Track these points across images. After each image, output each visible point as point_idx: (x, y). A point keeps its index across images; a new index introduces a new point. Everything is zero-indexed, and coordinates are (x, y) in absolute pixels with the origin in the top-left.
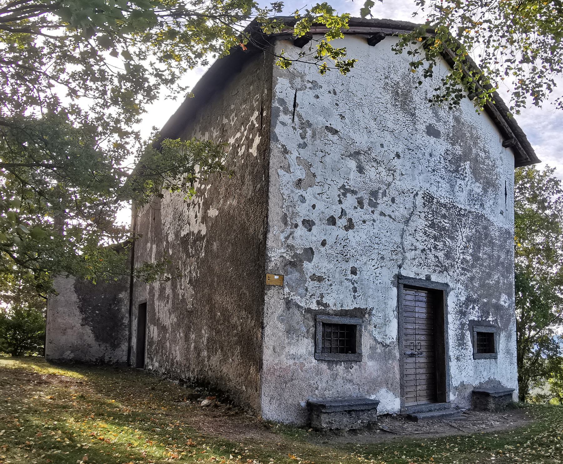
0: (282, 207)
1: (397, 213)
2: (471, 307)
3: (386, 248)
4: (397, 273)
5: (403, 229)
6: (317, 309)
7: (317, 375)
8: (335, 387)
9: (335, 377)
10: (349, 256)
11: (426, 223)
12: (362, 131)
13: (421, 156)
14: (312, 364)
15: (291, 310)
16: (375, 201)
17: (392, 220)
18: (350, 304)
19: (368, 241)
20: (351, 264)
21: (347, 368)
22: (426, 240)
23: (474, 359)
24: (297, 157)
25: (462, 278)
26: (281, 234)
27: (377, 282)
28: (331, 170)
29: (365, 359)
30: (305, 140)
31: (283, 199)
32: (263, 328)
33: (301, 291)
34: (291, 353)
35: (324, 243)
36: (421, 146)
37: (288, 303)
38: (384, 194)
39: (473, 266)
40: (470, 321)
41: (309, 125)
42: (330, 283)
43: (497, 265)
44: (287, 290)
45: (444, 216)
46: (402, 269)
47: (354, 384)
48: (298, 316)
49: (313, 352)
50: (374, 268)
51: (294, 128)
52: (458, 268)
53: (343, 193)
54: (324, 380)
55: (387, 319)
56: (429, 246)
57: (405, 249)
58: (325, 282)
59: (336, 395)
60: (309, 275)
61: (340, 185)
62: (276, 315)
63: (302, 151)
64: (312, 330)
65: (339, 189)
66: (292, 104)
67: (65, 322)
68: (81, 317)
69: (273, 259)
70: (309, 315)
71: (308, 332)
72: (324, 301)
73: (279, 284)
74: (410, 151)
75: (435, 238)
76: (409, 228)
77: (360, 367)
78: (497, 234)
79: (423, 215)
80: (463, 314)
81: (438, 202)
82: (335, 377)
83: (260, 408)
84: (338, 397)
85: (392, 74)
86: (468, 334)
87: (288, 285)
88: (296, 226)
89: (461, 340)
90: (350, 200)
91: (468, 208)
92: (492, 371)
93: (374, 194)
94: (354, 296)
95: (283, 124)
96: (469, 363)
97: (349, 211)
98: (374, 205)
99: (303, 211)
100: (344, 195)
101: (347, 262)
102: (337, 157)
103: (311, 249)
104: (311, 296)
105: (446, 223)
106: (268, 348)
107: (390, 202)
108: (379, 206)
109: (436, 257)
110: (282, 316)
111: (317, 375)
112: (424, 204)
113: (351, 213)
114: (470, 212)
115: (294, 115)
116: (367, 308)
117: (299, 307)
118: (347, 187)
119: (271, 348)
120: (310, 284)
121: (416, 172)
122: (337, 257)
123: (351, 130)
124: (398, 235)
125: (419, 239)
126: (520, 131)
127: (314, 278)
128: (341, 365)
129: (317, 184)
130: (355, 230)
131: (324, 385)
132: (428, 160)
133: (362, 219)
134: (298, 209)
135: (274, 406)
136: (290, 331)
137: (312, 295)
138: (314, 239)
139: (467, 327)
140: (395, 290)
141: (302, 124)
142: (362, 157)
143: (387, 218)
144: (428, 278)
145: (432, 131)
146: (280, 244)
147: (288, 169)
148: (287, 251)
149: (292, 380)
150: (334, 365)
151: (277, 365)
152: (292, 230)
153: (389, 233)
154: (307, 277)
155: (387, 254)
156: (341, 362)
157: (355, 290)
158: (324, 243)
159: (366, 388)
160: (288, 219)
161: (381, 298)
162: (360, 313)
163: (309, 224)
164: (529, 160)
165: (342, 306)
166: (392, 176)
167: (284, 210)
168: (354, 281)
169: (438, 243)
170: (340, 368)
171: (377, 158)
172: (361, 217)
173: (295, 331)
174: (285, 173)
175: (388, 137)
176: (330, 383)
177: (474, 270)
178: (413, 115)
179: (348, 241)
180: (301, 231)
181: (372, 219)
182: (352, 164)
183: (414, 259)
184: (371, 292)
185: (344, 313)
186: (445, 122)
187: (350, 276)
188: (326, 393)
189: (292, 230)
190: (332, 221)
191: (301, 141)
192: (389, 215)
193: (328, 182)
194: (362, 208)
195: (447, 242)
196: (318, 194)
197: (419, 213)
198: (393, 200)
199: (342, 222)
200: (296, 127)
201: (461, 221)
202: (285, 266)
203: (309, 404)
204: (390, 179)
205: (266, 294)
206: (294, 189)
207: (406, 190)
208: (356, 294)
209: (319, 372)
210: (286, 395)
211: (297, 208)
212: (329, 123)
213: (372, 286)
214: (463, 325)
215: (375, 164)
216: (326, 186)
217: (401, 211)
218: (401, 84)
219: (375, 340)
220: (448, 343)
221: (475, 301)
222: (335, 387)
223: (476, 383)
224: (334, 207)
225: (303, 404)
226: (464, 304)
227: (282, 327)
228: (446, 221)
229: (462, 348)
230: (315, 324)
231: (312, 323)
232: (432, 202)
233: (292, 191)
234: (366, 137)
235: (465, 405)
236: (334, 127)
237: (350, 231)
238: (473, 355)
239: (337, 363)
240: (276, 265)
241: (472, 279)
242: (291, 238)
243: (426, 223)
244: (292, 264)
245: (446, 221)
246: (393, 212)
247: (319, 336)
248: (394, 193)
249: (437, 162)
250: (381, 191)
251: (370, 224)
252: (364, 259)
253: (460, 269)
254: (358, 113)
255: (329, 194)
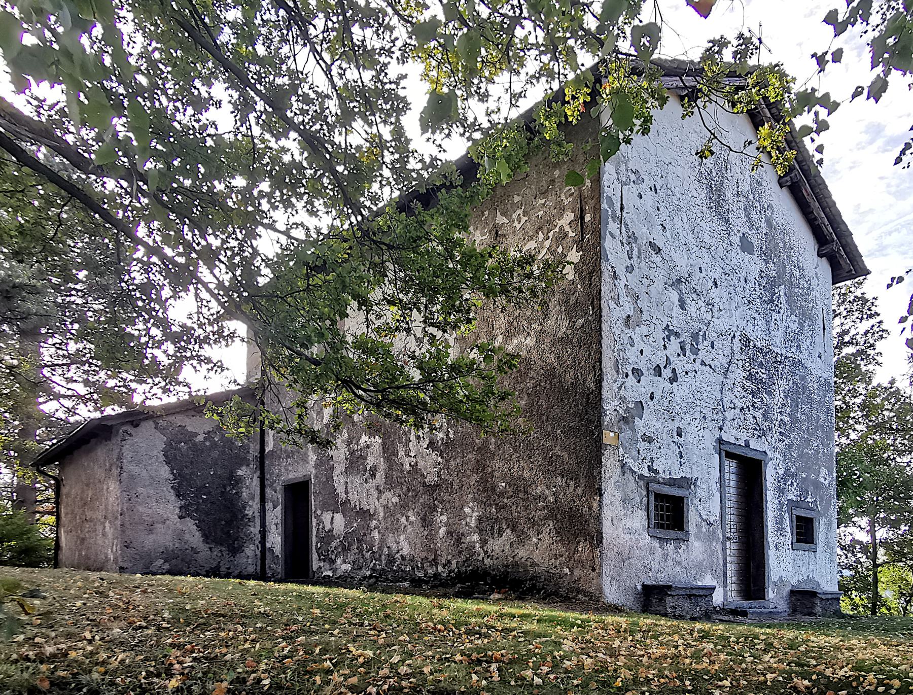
1: (716, 362)
2: (789, 483)
11: (744, 374)
17: (712, 371)
19: (691, 396)
20: (677, 424)
21: (676, 548)
25: (780, 445)
26: (614, 385)
29: (692, 538)
32: (601, 495)
33: (635, 453)
36: (736, 268)
39: (791, 430)
43: (817, 428)
45: (761, 365)
62: (613, 480)
67: (150, 511)
68: (178, 504)
69: (608, 412)
70: (641, 483)
75: (753, 393)
76: (728, 381)
78: (816, 386)
79: (740, 363)
80: (781, 491)
82: (666, 556)
83: (601, 590)
89: (779, 521)
90: (674, 345)
91: (784, 352)
92: (811, 567)
93: (695, 336)
94: (680, 462)
96: (788, 554)
98: (696, 351)
101: (673, 420)
103: (641, 402)
107: (710, 348)
109: (754, 417)
110: (618, 482)
112: (741, 349)
114: (786, 358)
117: (633, 472)
118: (671, 328)
120: (643, 445)
124: (718, 390)
125: (738, 394)
126: (844, 229)
132: (744, 288)
138: (644, 390)
139: (785, 508)
140: (717, 456)
145: (746, 246)
152: (623, 380)
153: (709, 388)
158: (652, 398)
160: (620, 367)
164: (853, 272)
169: (756, 400)
170: (670, 547)
177: (792, 436)
178: (727, 221)
179: (672, 395)
182: (675, 296)
183: (734, 420)
184: (695, 459)
185: (672, 482)
186: (758, 229)
187: (676, 439)
188: (659, 575)
189: (623, 380)
194: (684, 355)
197: (736, 362)
199: (667, 373)
201: (778, 371)
203: (645, 587)
204: (709, 318)
209: (652, 552)
210: (625, 575)
217: (721, 361)
221: (794, 476)
222: (666, 569)
223: (794, 581)
225: (639, 587)
226: (782, 479)
231: (644, 493)
232: (749, 346)
235: (783, 606)
238: (792, 544)
239: (667, 540)
241: (790, 446)
243: (744, 374)
244: (624, 419)
247: (652, 508)
249: (752, 289)
251: (693, 376)
253: (778, 434)
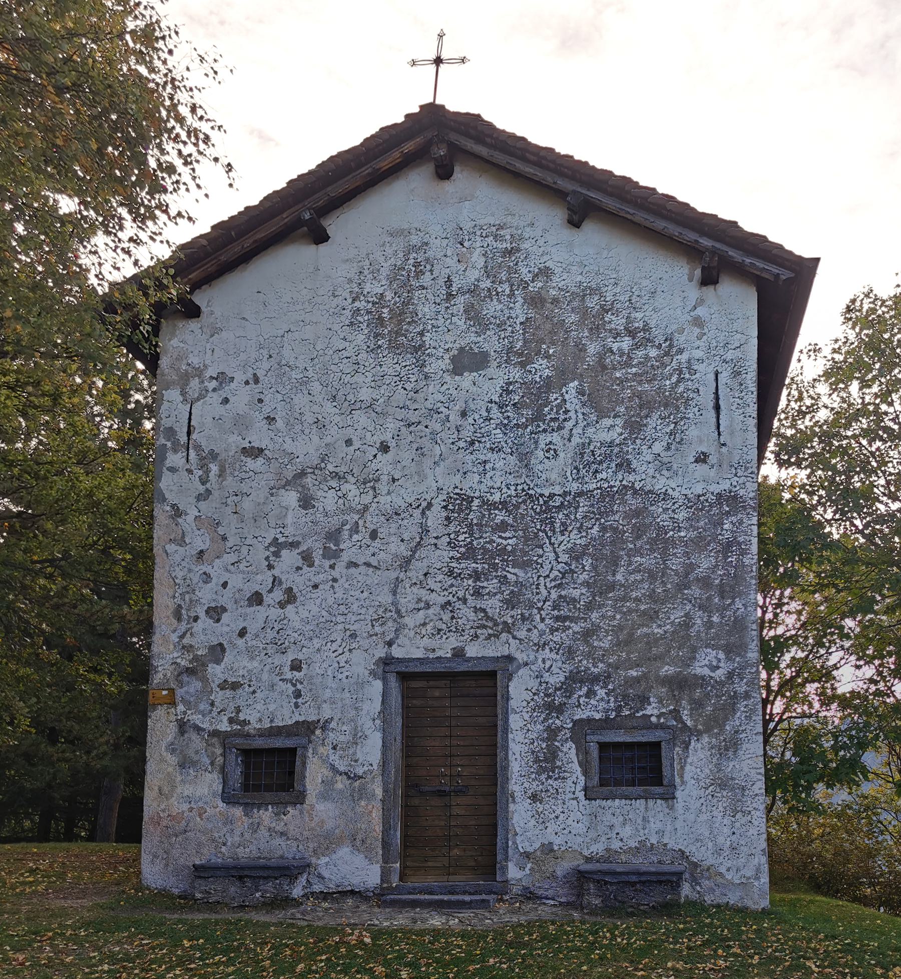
0: (174, 597)
3: (362, 617)
4: (383, 655)
5: (397, 578)
6: (229, 729)
7: (225, 824)
8: (255, 842)
9: (255, 828)
10: (287, 643)
12: (307, 431)
13: (438, 427)
14: (218, 810)
15: (186, 735)
16: (334, 548)
18: (287, 717)
19: (324, 613)
20: (290, 656)
22: (452, 586)
23: (587, 798)
24: (196, 517)
27: (340, 676)
28: (253, 521)
29: (311, 798)
30: (208, 485)
31: (176, 584)
34: (186, 794)
35: (242, 633)
37: (183, 726)
38: (355, 529)
40: (575, 723)
41: (213, 456)
42: (251, 689)
44: (181, 708)
45: (503, 526)
46: (394, 646)
47: (288, 839)
48: (196, 742)
49: (220, 792)
50: (336, 654)
51: (190, 471)
52: (543, 620)
53: (273, 553)
54: (238, 832)
55: (360, 734)
56: (460, 594)
57: (403, 610)
58: (244, 688)
59: (255, 854)
60: (217, 683)
61: (269, 540)
63: (203, 505)
64: (220, 760)
65: (267, 548)
66: (185, 430)
71: (212, 764)
72: (242, 717)
73: (169, 701)
74: (412, 428)
77: (301, 812)
81: (484, 503)
84: (259, 858)
85: (368, 285)
86: (569, 752)
87: (183, 700)
88: (196, 619)
93: (334, 536)
95: (172, 470)
97: (287, 576)
98: (331, 555)
99: (206, 595)
100: (277, 554)
102: (263, 493)
103: (221, 645)
104: (219, 713)
105: (506, 539)
106: (152, 789)
108: (344, 554)
110: (172, 744)
111: (225, 824)
113: (291, 579)
115: (188, 450)
116: (319, 721)
117: (198, 729)
119: (156, 788)
120: (219, 696)
121: (428, 462)
122: (265, 649)
123: (286, 439)
127: (223, 686)
128: (267, 810)
129: (228, 550)
130: (298, 604)
131: (237, 839)
133: (312, 583)
134: (200, 595)
135: (159, 866)
136: (184, 764)
137: (221, 711)
140: (378, 685)
141: (202, 459)
142: (309, 480)
143: (363, 569)
144: (459, 653)
146: (172, 647)
147: (181, 541)
148: (183, 654)
149: (186, 831)
150: (255, 811)
151: (163, 811)
152: (189, 626)
153: (366, 594)
154: (214, 686)
155: (362, 628)
156: (267, 805)
157: (298, 694)
159: (311, 845)
160: (184, 612)
161: (348, 701)
162: (306, 729)
163: (216, 613)
165: (272, 721)
166: (371, 492)
167: (178, 600)
168: (297, 680)
170: (266, 816)
171: (337, 470)
172: (310, 580)
173: (194, 764)
174: (178, 548)
175: (362, 419)
176: (247, 836)
179: (285, 622)
180: (205, 622)
181: (331, 578)
182: (291, 498)
183: (424, 624)
185: (275, 732)
188: (240, 850)
189: (189, 626)
190: (257, 599)
191: (202, 489)
192: (365, 563)
193: (248, 542)
194: (311, 565)
195: (509, 576)
196: (233, 564)
198: (374, 535)
200: (192, 468)
201: (552, 523)
202: (179, 675)
204: (367, 499)
205: (150, 717)
206: (193, 567)
207: (404, 505)
208: (300, 700)
211: (197, 593)
212: (247, 440)
213: (330, 682)
214: (552, 733)
215: (334, 483)
216: (244, 550)
218: (389, 295)
219: (333, 768)
220: (506, 768)
224: (259, 577)
227: (172, 760)
228: (507, 535)
229: (550, 777)
230: (224, 752)
233: (190, 571)
234: (316, 439)
236: (256, 444)
237: (290, 607)
240: (165, 676)
242: (188, 635)
244: (190, 671)
245: (507, 535)
246: (373, 555)
248: (375, 520)
250: (348, 527)
252: (317, 643)
254: (300, 400)
255: (251, 560)
